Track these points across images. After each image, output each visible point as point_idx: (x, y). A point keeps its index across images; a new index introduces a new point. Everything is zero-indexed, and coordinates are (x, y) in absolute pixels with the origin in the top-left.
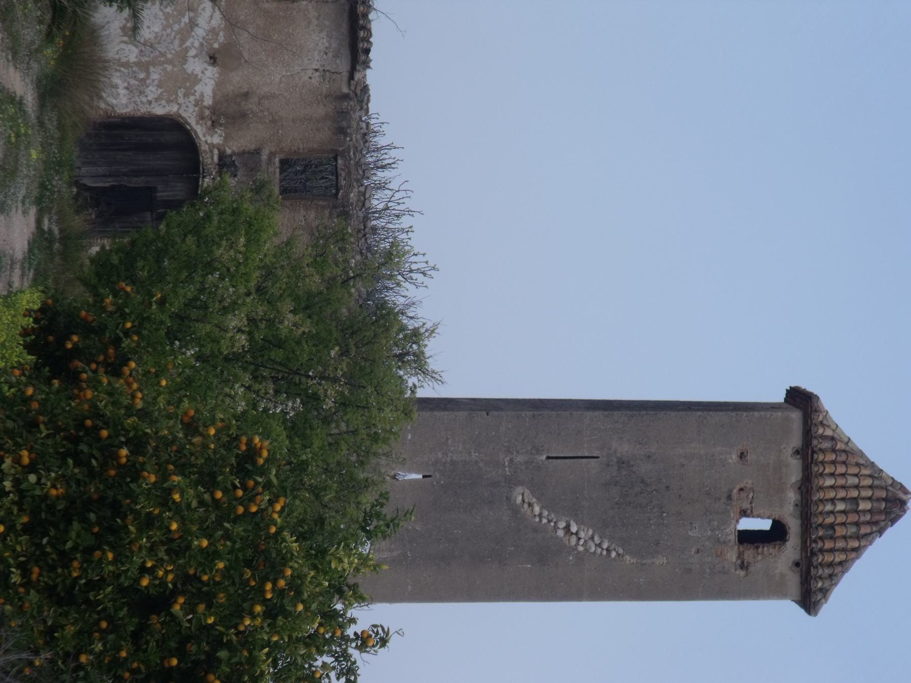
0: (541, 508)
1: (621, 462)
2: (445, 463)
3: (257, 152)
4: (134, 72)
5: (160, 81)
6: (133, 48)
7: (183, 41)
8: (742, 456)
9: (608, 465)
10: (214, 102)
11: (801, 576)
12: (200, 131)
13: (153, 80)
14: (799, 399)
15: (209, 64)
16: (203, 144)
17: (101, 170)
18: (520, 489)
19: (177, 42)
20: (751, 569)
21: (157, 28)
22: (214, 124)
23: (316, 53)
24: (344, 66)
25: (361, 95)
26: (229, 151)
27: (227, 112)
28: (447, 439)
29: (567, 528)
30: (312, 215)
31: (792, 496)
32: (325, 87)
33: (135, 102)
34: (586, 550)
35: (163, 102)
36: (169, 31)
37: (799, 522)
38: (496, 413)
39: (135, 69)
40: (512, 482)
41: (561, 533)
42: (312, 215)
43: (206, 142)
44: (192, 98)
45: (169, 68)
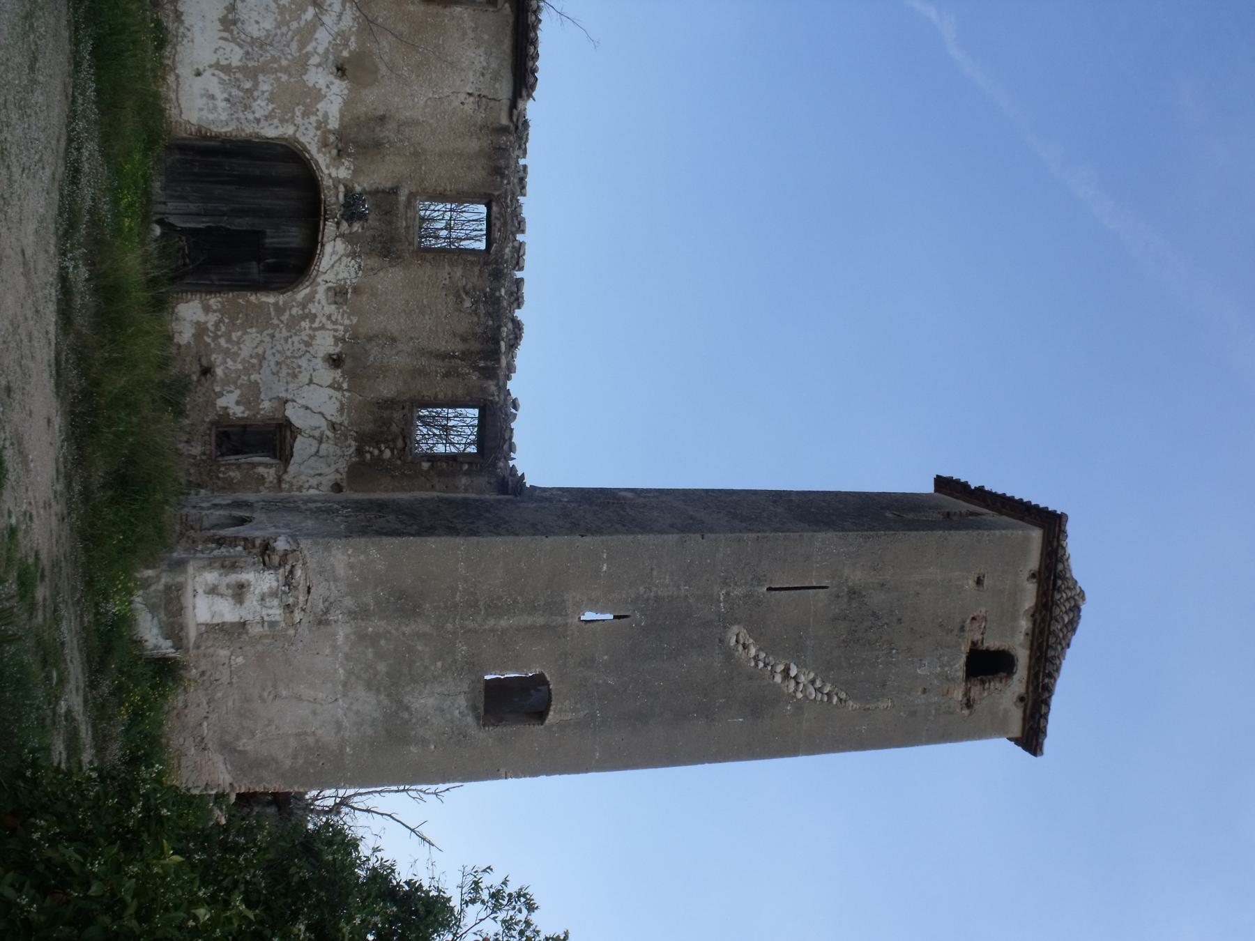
0: (758, 650)
1: (853, 593)
2: (648, 599)
3: (394, 191)
4: (238, 80)
5: (272, 93)
6: (237, 48)
7: (303, 45)
8: (979, 582)
9: (838, 596)
10: (341, 124)
11: (1024, 712)
12: (322, 161)
13: (263, 92)
14: (943, 484)
15: (336, 77)
16: (326, 178)
17: (193, 207)
18: (735, 629)
19: (294, 45)
20: (976, 707)
21: (268, 24)
22: (341, 153)
23: (471, 73)
24: (504, 90)
25: (518, 129)
26: (358, 189)
27: (356, 140)
28: (652, 569)
29: (786, 671)
30: (459, 272)
31: (1024, 624)
32: (481, 115)
33: (238, 119)
34: (806, 697)
35: (276, 122)
36: (284, 29)
37: (1027, 652)
38: (712, 536)
39: (237, 75)
40: (727, 620)
41: (778, 679)
42: (459, 272)
43: (330, 175)
44: (313, 119)
45: (284, 78)
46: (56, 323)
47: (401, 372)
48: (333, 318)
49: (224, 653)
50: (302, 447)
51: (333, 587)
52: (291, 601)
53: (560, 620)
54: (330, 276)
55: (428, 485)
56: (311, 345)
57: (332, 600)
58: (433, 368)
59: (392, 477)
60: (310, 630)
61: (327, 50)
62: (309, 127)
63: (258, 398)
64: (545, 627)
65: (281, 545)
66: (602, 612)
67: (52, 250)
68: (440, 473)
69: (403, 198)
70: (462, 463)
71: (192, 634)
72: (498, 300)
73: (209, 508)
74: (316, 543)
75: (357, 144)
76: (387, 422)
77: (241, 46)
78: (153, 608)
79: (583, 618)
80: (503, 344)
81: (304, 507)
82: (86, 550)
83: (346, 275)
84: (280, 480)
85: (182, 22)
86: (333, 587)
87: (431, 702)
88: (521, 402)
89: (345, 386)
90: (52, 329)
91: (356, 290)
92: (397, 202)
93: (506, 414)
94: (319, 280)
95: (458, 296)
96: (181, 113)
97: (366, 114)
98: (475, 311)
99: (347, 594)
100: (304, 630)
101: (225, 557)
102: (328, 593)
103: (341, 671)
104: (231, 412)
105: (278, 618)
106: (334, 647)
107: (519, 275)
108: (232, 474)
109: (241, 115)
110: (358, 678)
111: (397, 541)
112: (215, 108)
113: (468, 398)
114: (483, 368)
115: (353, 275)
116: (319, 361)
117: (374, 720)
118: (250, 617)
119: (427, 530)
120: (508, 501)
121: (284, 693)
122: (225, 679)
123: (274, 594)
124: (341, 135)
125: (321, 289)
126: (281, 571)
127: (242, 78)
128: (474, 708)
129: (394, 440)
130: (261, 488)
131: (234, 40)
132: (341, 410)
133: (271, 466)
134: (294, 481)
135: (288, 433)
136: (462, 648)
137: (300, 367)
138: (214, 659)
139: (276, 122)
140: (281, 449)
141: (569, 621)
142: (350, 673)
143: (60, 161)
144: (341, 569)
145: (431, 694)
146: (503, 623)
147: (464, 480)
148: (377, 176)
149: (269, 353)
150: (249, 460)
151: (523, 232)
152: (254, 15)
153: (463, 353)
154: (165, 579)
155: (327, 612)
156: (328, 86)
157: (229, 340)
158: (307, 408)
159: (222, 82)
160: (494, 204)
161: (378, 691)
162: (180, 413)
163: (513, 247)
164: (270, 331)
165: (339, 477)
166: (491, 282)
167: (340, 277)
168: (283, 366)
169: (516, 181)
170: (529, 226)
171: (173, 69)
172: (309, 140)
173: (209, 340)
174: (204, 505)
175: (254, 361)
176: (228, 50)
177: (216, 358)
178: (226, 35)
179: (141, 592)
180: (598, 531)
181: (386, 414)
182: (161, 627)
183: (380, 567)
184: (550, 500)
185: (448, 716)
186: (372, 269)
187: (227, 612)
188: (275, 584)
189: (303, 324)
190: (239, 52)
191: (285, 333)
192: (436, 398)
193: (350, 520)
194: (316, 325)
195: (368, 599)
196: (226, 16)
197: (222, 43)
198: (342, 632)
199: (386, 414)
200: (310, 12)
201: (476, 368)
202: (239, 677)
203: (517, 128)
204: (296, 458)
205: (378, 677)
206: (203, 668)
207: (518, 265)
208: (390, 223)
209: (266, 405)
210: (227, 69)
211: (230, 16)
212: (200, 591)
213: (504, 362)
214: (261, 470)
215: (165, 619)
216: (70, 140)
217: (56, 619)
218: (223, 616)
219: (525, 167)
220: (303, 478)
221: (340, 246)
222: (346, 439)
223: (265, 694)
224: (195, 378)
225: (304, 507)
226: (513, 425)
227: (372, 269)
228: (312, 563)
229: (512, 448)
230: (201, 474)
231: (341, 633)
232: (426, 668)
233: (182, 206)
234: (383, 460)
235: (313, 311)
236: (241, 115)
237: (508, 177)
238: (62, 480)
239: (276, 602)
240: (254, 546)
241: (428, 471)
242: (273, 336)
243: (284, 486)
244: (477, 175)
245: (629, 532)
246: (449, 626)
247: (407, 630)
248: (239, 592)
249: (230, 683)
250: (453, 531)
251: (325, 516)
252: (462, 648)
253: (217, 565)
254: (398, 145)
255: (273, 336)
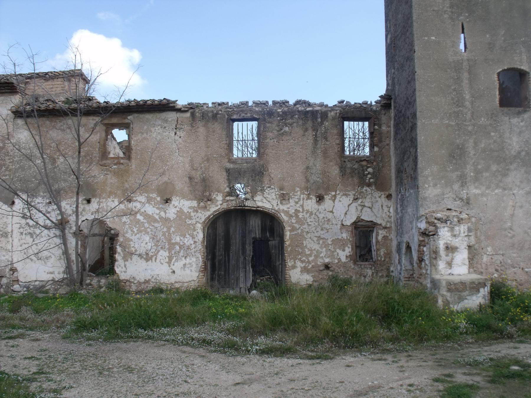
2: (452, 12)
3: (228, 171)
6: (160, 253)
7: (155, 221)
10: (195, 200)
13: (181, 240)
15: (170, 203)
16: (223, 207)
17: (242, 275)
19: (156, 225)
21: (147, 238)
26: (228, 189)
27: (202, 191)
28: (434, 10)
30: (270, 134)
33: (195, 252)
35: (195, 233)
36: (149, 230)
42: (270, 134)
43: (221, 204)
44: (192, 214)
45: (173, 229)
46: (288, 358)
47: (325, 164)
48: (297, 200)
49: (485, 259)
50: (367, 216)
51: (447, 196)
52: (456, 220)
53: (465, 64)
54: (275, 203)
55: (387, 147)
56: (312, 212)
57: (455, 197)
58: (323, 146)
59: (383, 167)
60: (472, 209)
61: (158, 208)
62: (196, 216)
63: (341, 240)
64: (470, 72)
65: (423, 225)
66: (460, 39)
67: (244, 359)
68: (380, 141)
69: (231, 166)
70: (374, 129)
71: (475, 277)
72: (284, 113)
73: (401, 266)
74: (422, 206)
75: (204, 191)
76: (353, 170)
77: (159, 251)
78: (461, 299)
79: (463, 51)
80: (308, 109)
81: (400, 214)
82: (428, 340)
83: (273, 195)
84: (385, 228)
85: (149, 280)
86: (447, 196)
87: (515, 139)
88: (340, 99)
89: (333, 193)
90: (291, 361)
91: (281, 189)
92: (234, 169)
93: (347, 106)
94: (277, 209)
95: (283, 134)
96: (193, 280)
97: (188, 187)
98: (291, 125)
99: (452, 188)
100: (472, 213)
101: (430, 257)
102: (451, 199)
103: (496, 191)
104: (348, 254)
105: (466, 227)
106: (482, 195)
107: (270, 103)
108: (382, 253)
109: (193, 251)
110: (501, 181)
111: (420, 159)
112: (190, 264)
113: (338, 127)
114: (321, 120)
115: (273, 190)
116: (320, 207)
117: (526, 172)
118: (465, 244)
119: (414, 143)
120: (395, 102)
121: (509, 224)
122: (500, 258)
123: (452, 229)
124: (200, 200)
125: (282, 207)
126: (438, 225)
127: (174, 251)
128: (519, 113)
129: (362, 166)
130: (390, 238)
131: (156, 255)
132: (347, 195)
133: (377, 232)
134: (386, 220)
135: (359, 223)
136: (483, 121)
137: (324, 218)
138: (489, 264)
139: (195, 233)
140: (369, 227)
141: (465, 58)
142: (497, 186)
143: (197, 351)
144: (438, 191)
145: (510, 138)
146: (467, 97)
147: (384, 128)
148: (220, 179)
149: (316, 234)
150: (374, 244)
151: (247, 102)
152: (143, 245)
153: (314, 130)
154: (444, 292)
155: (462, 199)
156: (176, 207)
157: (310, 255)
158: (346, 214)
159: (177, 260)
160: (232, 118)
161: (508, 170)
162: (347, 282)
163: (255, 106)
164: (305, 234)
165: (383, 196)
166: (274, 117)
167: (274, 197)
168: (323, 227)
169: (220, 107)
170: (244, 100)
171: (172, 284)
172: (204, 216)
173: (310, 266)
174: (399, 268)
175: (321, 242)
176: (161, 258)
177: (320, 262)
178: (154, 259)
179: (451, 306)
180: (412, 44)
181: (348, 171)
182: (473, 294)
183: (435, 168)
184: (393, 79)
185: (524, 129)
186: (270, 181)
187: (462, 256)
188: (446, 229)
189: (300, 216)
190: (162, 252)
191: (306, 226)
192: (339, 144)
193: (407, 187)
194: (301, 210)
195: (454, 175)
196: (144, 259)
197: (158, 261)
198: (474, 190)
199: (348, 171)
200: (139, 217)
201: (322, 123)
202: (499, 250)
203: (191, 108)
204: (373, 219)
205: (500, 169)
206: (494, 270)
207: (266, 103)
208: (245, 172)
209: (345, 235)
210: (170, 258)
211: (145, 257)
212: (450, 271)
213: (318, 108)
214: (380, 238)
215: (467, 292)
216: (187, 344)
217: (476, 364)
218: (464, 259)
219: (213, 103)
220: (384, 215)
221: (258, 198)
222: (362, 192)
223: (509, 235)
224: (331, 273)
225: (400, 214)
226: (353, 103)
227: (270, 181)
228: (434, 208)
229: (366, 103)
230: (382, 270)
231: (474, 191)
232: (495, 142)
233: (242, 279)
234: (374, 172)
235: (293, 211)
236: (193, 251)
237: (217, 111)
238: (385, 356)
239: (457, 228)
240: (423, 241)
241: (379, 148)
242: (308, 232)
243: (388, 226)
244: (217, 127)
245: (411, 26)
246: (470, 128)
247: (472, 153)
248: (450, 249)
249: (503, 255)
250: (414, 127)
251: (405, 202)
252: (483, 121)
253: (434, 262)
254: (203, 169)
255: (308, 232)
